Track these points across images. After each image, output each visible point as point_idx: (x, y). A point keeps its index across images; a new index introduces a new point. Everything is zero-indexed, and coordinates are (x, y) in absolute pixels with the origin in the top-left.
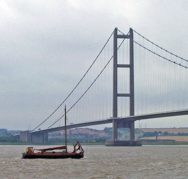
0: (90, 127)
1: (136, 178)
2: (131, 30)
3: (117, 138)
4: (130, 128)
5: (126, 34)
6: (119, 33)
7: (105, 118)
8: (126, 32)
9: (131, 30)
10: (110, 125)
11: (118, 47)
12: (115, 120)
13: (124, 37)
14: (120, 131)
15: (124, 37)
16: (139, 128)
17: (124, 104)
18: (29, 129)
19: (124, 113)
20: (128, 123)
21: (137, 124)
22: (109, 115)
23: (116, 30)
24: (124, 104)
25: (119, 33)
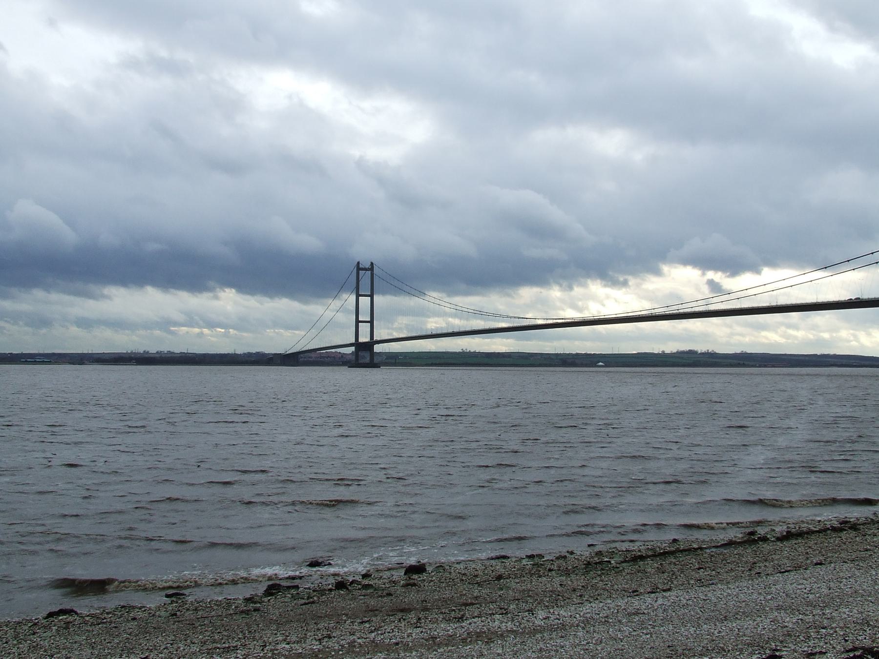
0: (339, 350)
1: (534, 655)
2: (372, 264)
3: (358, 361)
4: (370, 351)
5: (367, 267)
6: (361, 266)
7: (349, 342)
8: (368, 266)
9: (372, 264)
10: (353, 349)
11: (363, 267)
12: (356, 344)
13: (365, 269)
14: (361, 353)
15: (365, 269)
16: (382, 351)
17: (364, 329)
18: (384, 350)
19: (364, 338)
20: (368, 347)
21: (377, 348)
22: (353, 341)
23: (358, 263)
24: (364, 329)
25: (361, 266)
